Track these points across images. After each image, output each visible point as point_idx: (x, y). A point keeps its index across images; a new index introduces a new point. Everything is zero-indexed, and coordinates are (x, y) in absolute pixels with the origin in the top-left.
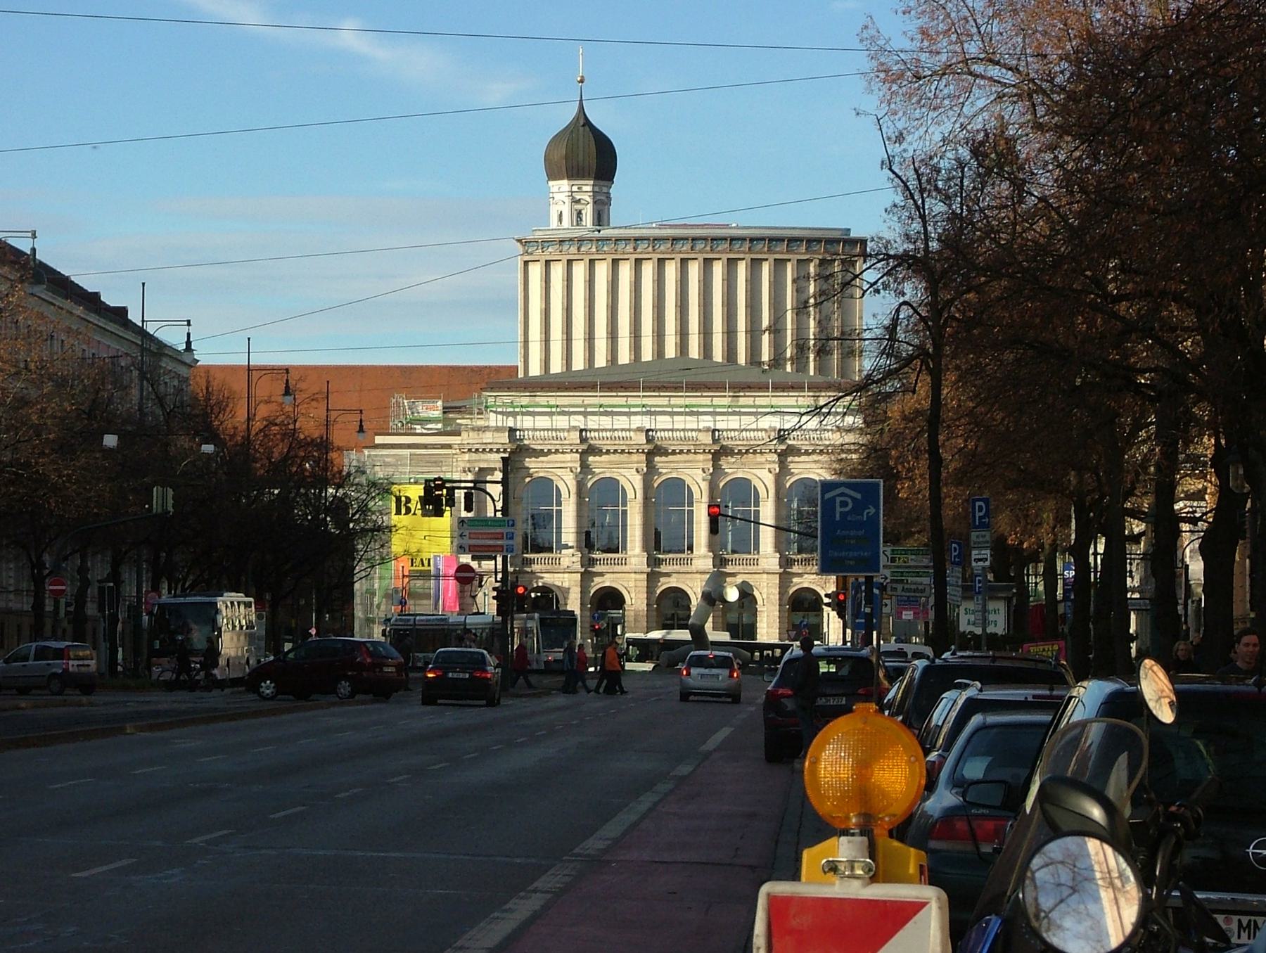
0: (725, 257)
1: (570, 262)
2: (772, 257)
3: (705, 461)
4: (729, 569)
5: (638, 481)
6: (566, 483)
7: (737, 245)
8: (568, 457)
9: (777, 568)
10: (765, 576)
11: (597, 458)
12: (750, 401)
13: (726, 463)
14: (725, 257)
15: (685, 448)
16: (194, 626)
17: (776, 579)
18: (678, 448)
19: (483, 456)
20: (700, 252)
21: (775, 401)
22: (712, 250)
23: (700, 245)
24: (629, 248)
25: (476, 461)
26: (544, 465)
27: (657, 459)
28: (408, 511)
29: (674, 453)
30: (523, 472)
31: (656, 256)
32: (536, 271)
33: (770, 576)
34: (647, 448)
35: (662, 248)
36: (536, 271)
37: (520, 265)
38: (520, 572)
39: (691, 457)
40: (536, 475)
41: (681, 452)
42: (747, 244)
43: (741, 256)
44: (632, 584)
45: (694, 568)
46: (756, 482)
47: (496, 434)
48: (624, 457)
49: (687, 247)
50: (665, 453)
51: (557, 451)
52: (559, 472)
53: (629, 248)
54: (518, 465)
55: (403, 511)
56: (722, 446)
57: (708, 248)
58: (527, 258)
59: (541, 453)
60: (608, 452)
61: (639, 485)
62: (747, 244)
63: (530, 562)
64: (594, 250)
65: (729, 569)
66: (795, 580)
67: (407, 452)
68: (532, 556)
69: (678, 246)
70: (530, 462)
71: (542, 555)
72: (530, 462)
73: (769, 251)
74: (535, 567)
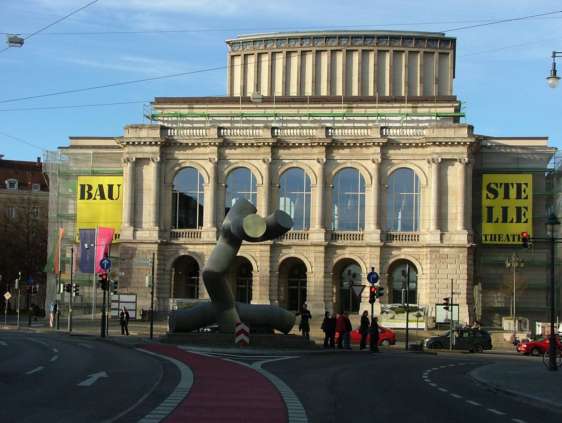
0: (360, 49)
1: (259, 55)
2: (392, 49)
3: (319, 153)
4: (339, 243)
5: (264, 168)
6: (206, 169)
7: (369, 41)
8: (208, 150)
9: (378, 242)
10: (368, 249)
11: (233, 151)
12: (362, 111)
13: (339, 155)
14: (360, 49)
15: (303, 142)
16: (545, 306)
17: (377, 251)
18: (297, 142)
19: (139, 149)
20: (344, 46)
21: (380, 111)
22: (352, 45)
23: (344, 42)
24: (298, 44)
25: (134, 153)
26: (189, 157)
27: (281, 151)
28: (90, 196)
29: (294, 146)
30: (173, 162)
31: (314, 49)
32: (238, 61)
33: (373, 249)
34: (271, 141)
35: (319, 44)
36: (238, 61)
37: (229, 58)
38: (167, 244)
39: (308, 150)
40: (183, 166)
41: (300, 146)
42: (375, 41)
43: (371, 48)
44: (258, 254)
45: (309, 242)
46: (362, 171)
47: (150, 131)
48: (254, 150)
49: (336, 42)
50: (288, 146)
51: (199, 145)
52: (201, 163)
53: (298, 44)
54: (169, 157)
55: (86, 197)
56: (334, 140)
57: (349, 44)
58: (233, 54)
59: (186, 146)
60: (240, 146)
61: (265, 173)
62: (375, 41)
63: (177, 236)
64: (275, 46)
65: (339, 243)
66: (394, 252)
67: (91, 151)
68: (178, 230)
69: (330, 42)
70: (179, 155)
71: (186, 230)
72: (179, 155)
73: (390, 46)
74: (181, 240)
